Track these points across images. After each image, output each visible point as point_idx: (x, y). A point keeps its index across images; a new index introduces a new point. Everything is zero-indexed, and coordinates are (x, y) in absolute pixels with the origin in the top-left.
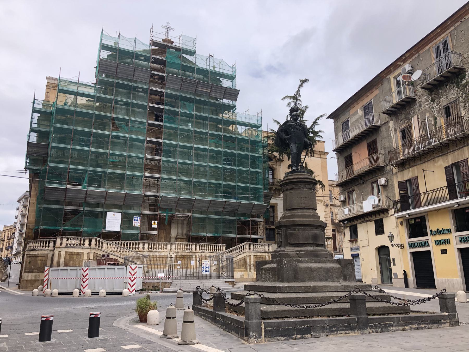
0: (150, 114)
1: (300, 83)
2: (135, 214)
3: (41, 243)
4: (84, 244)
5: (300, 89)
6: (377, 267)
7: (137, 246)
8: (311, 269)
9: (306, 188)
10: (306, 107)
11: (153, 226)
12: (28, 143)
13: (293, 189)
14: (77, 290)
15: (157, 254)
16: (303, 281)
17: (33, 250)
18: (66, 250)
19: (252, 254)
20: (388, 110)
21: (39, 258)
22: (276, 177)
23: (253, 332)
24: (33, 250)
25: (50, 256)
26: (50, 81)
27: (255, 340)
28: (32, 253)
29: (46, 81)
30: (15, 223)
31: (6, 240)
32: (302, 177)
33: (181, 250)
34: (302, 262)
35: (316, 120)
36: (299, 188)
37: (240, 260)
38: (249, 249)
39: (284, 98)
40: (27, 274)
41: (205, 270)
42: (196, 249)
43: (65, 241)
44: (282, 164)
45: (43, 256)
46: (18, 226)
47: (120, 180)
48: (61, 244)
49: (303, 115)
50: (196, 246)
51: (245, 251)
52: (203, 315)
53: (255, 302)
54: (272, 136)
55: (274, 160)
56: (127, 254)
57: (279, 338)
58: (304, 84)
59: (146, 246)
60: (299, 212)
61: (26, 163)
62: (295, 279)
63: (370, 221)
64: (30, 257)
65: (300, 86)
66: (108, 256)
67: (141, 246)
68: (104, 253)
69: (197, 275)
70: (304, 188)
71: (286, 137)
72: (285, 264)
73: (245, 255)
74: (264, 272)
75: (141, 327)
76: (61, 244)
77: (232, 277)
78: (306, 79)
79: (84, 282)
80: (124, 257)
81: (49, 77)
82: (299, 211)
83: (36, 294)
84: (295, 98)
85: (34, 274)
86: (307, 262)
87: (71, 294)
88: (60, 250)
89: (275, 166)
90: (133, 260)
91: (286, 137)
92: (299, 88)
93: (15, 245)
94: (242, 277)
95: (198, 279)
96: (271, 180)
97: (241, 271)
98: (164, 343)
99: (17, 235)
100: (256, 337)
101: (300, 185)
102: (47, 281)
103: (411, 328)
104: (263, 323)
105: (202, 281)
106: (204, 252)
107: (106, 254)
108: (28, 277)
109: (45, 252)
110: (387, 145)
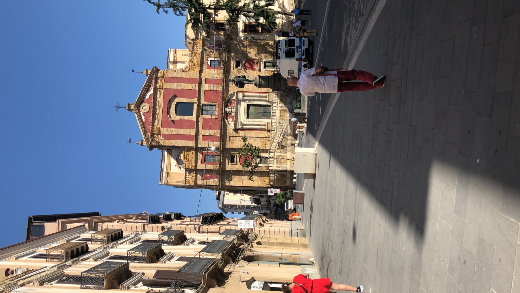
84: (159, 6)
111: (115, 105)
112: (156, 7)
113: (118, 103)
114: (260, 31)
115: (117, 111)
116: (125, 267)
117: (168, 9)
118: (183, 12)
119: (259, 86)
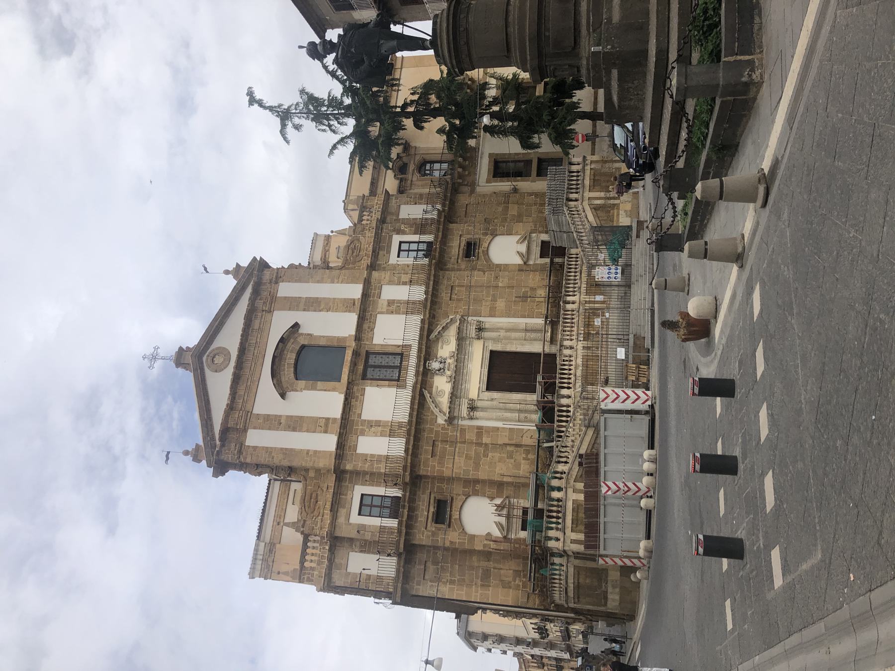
1: (256, 106)
3: (554, 579)
4: (559, 500)
5: (267, 105)
7: (564, 409)
9: (467, 17)
10: (302, 92)
13: (467, 43)
14: (643, 502)
15: (579, 373)
16: (647, 13)
17: (566, 593)
18: (568, 531)
19: (587, 194)
21: (581, 580)
22: (438, 158)
23: (742, 76)
24: (566, 593)
25: (577, 562)
26: (258, 573)
27: (758, 73)
29: (257, 579)
30: (515, 654)
32: (445, 25)
33: (575, 329)
34: (610, 19)
35: (328, 71)
36: (466, 29)
37: (596, 216)
38: (576, 200)
39: (285, 139)
40: (609, 603)
41: (613, 276)
42: (573, 303)
44: (413, 144)
45: (579, 574)
46: (520, 649)
48: (557, 539)
49: (317, 99)
50: (569, 303)
51: (580, 208)
52: (702, 221)
53: (684, 76)
55: (405, 160)
57: (756, 27)
58: (258, 96)
59: (564, 392)
60: (514, 30)
62: (643, 28)
64: (578, 598)
65: (261, 104)
66: (581, 456)
67: (564, 401)
68: (577, 463)
69: (623, 289)
70: (467, 21)
71: (367, 63)
72: (613, 47)
73: (587, 208)
74: (627, 103)
75: (717, 330)
76: (557, 539)
77: (630, 228)
78: (248, 94)
79: (629, 489)
80: (584, 429)
81: (249, 574)
82: (511, 29)
84: (284, 115)
85: (610, 590)
86: (610, 10)
87: (649, 513)
89: (418, 158)
91: (367, 63)
92: (265, 108)
93: (553, 653)
94: (629, 214)
95: (629, 286)
96: (445, 166)
97: (618, 215)
98: (751, 258)
99: (537, 651)
100: (753, 70)
101: (462, 29)
102: (624, 560)
104: (726, 59)
105: (633, 279)
106: (580, 288)
108: (613, 600)
109: (571, 570)
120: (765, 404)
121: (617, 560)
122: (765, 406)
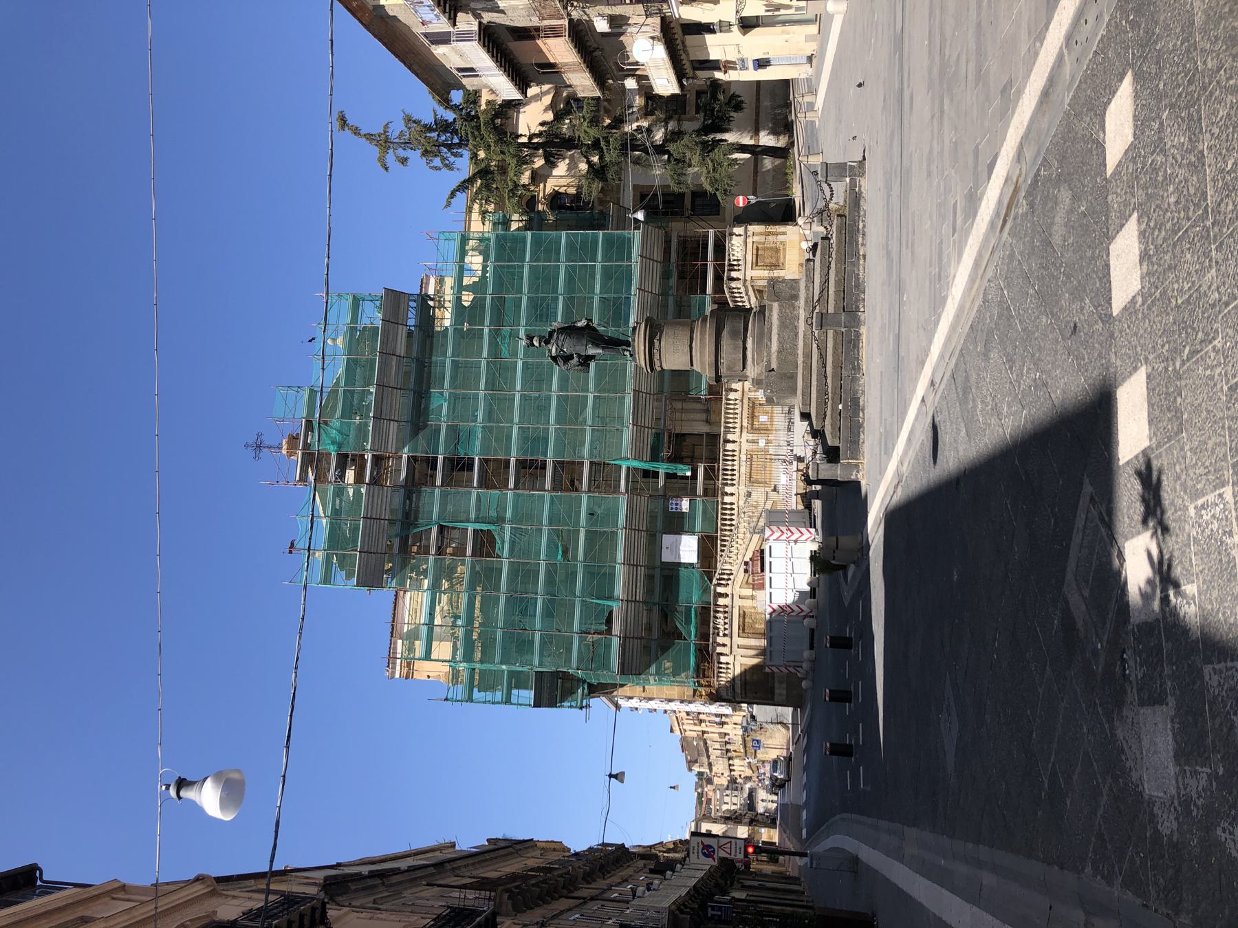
0: (459, 484)
2: (666, 508)
6: (783, 32)
8: (779, 352)
11: (689, 474)
12: (538, 704)
20: (450, 18)
28: (738, 690)
31: (703, 727)
33: (738, 421)
43: (720, 640)
47: (599, 542)
54: (481, 206)
56: (742, 530)
59: (728, 489)
61: (571, 707)
62: (793, 377)
63: (683, 43)
65: (356, 132)
66: (746, 563)
68: (742, 570)
80: (748, 535)
83: (810, 683)
84: (384, 142)
85: (776, 685)
88: (735, 647)
90: (755, 519)
103: (863, 245)
107: (743, 567)
108: (781, 695)
110: (524, 13)
111: (252, 439)
112: (375, 151)
113: (260, 435)
114: (762, 794)
115: (257, 457)
116: (657, 573)
117: (408, 153)
118: (452, 159)
119: (537, 29)
120: (1128, 80)
121: (783, 669)
122: (1126, 88)
